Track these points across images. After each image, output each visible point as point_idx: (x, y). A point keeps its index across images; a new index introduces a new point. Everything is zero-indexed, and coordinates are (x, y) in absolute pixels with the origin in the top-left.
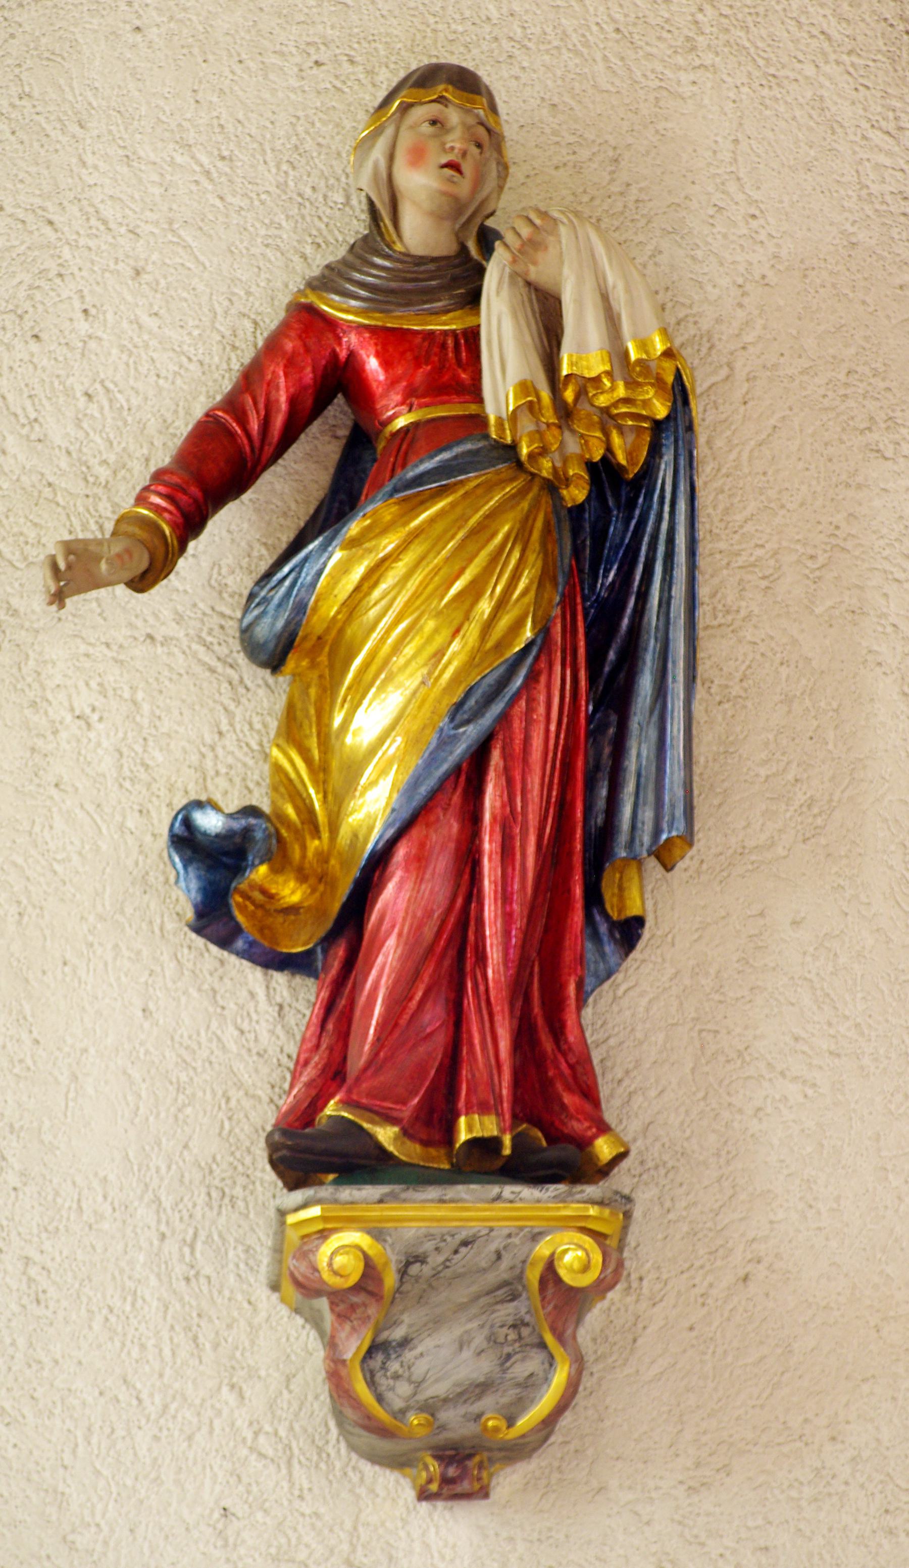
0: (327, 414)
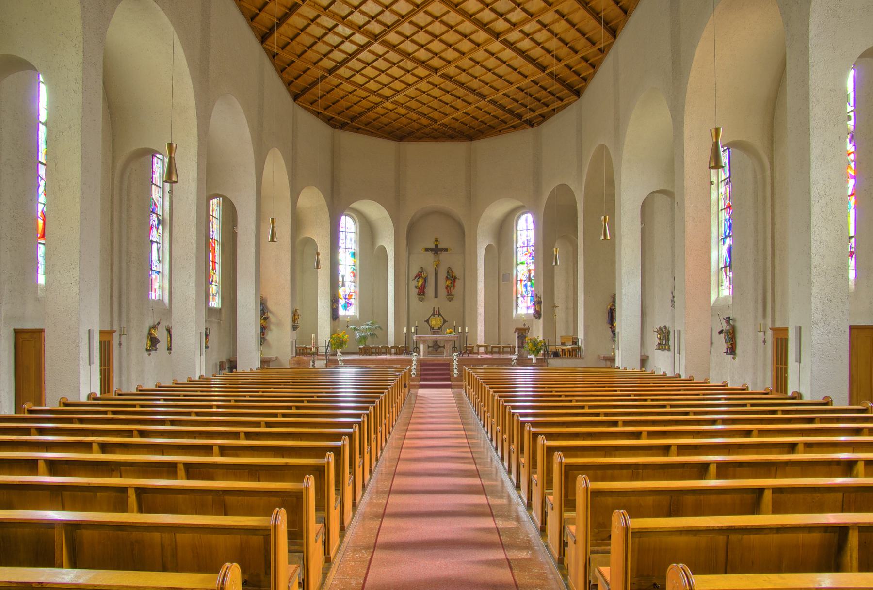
0: (419, 276)
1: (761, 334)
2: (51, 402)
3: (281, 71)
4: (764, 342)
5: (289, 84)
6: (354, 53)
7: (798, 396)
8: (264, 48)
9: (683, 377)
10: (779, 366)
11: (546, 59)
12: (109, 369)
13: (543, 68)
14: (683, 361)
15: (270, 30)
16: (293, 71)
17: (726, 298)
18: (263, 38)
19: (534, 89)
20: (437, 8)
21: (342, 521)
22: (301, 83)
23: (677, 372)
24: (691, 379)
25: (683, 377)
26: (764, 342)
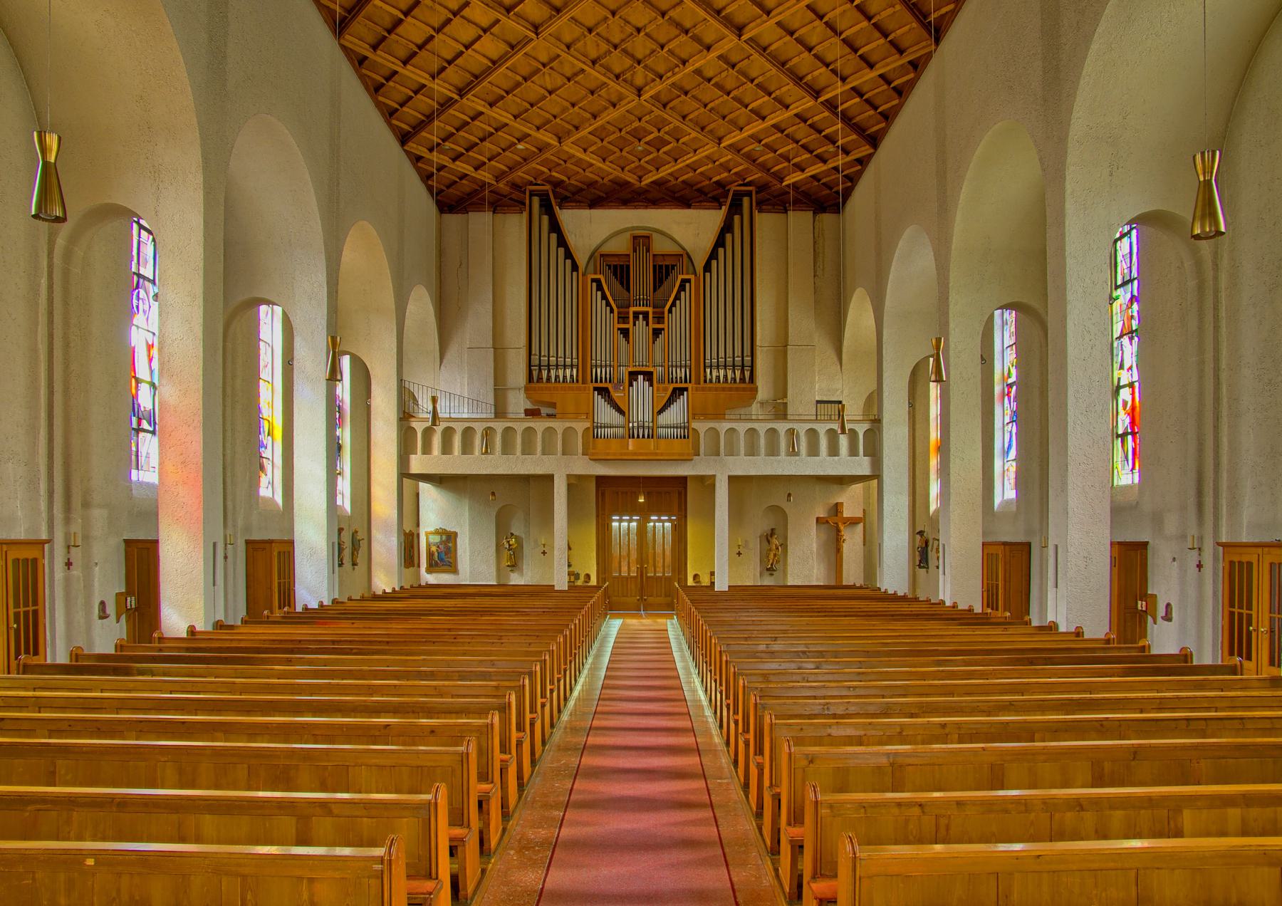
1: (1195, 552)
2: (299, 609)
3: (375, 89)
4: (1199, 566)
5: (389, 114)
6: (501, 58)
7: (1052, 627)
8: (344, 48)
9: (1062, 629)
10: (1245, 611)
11: (820, 75)
12: (36, 613)
13: (816, 93)
14: (948, 586)
15: (349, 12)
16: (397, 91)
17: (1009, 502)
18: (403, 139)
19: (801, 131)
20: (639, 14)
21: (520, 777)
22: (412, 113)
23: (1051, 617)
24: (1078, 633)
25: (1062, 629)
26: (1199, 566)
